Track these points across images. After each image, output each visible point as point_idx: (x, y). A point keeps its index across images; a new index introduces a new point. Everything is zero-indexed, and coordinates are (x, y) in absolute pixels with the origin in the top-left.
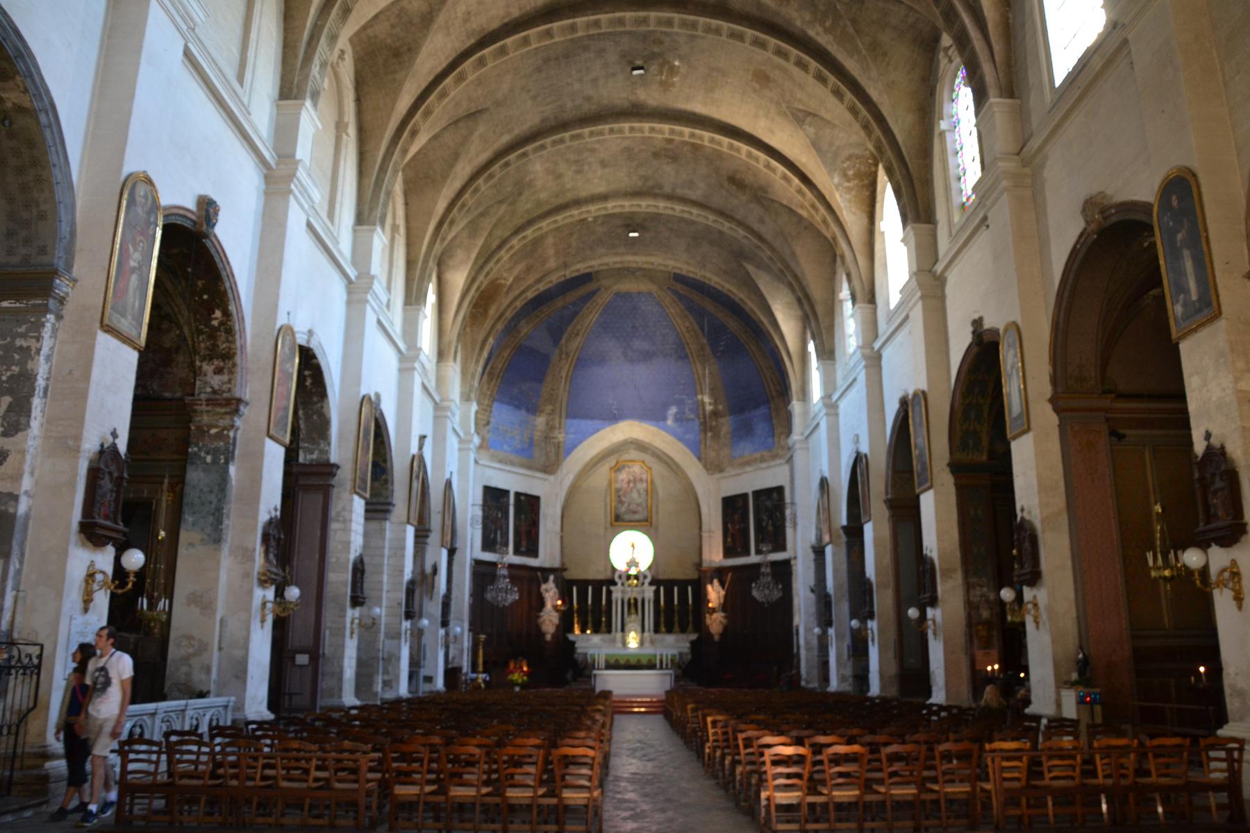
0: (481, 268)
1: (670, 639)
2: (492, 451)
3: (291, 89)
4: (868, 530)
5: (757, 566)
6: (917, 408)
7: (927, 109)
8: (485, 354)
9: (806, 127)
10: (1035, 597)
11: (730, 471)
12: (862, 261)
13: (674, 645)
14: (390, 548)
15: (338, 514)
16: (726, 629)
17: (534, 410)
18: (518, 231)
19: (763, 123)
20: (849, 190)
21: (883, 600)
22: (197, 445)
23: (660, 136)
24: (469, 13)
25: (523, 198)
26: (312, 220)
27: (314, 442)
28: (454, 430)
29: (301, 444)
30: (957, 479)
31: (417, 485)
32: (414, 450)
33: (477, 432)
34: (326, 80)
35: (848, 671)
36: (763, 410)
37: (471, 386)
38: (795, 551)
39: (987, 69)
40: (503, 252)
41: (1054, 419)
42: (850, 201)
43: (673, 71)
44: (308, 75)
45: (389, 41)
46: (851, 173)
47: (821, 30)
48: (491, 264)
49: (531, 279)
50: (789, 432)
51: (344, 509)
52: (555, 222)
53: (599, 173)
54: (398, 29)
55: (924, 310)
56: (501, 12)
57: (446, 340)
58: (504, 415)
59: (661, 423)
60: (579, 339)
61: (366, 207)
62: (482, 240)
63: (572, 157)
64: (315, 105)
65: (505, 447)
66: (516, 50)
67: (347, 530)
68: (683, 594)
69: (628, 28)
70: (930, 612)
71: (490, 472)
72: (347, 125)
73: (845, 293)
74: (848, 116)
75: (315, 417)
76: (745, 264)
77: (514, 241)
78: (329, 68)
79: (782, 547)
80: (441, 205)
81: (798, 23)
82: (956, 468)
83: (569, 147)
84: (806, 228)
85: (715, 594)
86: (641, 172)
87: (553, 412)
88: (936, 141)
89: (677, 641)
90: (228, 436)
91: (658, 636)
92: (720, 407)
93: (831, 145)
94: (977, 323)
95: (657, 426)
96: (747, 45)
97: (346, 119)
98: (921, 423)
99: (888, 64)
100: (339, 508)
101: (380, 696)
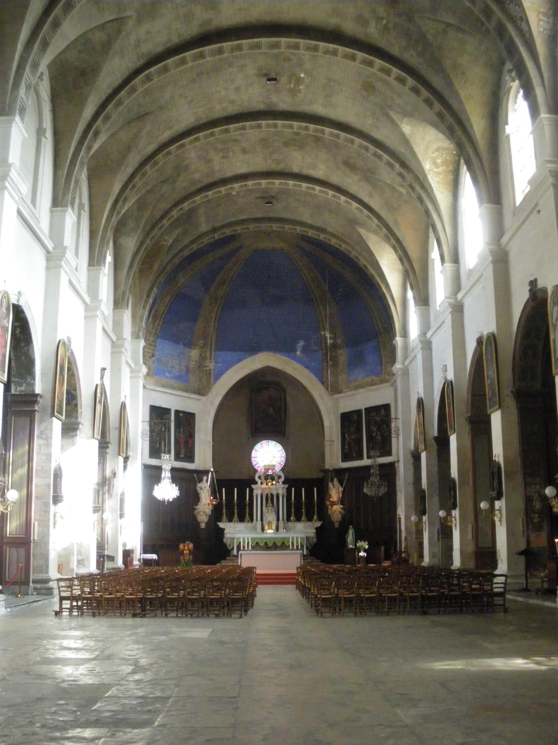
0: (147, 234)
1: (300, 526)
2: (156, 377)
4: (453, 439)
5: (367, 468)
8: (151, 301)
13: (302, 531)
16: (343, 517)
17: (189, 344)
18: (176, 205)
19: (370, 121)
20: (438, 174)
23: (290, 130)
25: (181, 178)
26: (21, 208)
28: (127, 362)
31: (99, 408)
32: (98, 381)
33: (145, 363)
34: (30, 99)
35: (438, 550)
37: (140, 327)
38: (398, 457)
39: (539, 91)
40: (165, 221)
42: (439, 183)
43: (299, 81)
44: (16, 97)
46: (439, 161)
47: (414, 54)
49: (186, 241)
50: (393, 360)
58: (166, 349)
59: (292, 354)
60: (225, 287)
61: (61, 193)
64: (22, 119)
65: (167, 374)
66: (176, 68)
68: (310, 495)
69: (264, 50)
71: (155, 395)
72: (45, 131)
73: (435, 255)
75: (23, 358)
78: (32, 90)
79: (389, 453)
80: (117, 188)
83: (217, 139)
85: (335, 492)
86: (274, 157)
87: (205, 346)
89: (305, 527)
91: (290, 524)
94: (533, 283)
95: (289, 357)
97: (44, 126)
98: (492, 360)
99: (466, 82)
101: (75, 572)
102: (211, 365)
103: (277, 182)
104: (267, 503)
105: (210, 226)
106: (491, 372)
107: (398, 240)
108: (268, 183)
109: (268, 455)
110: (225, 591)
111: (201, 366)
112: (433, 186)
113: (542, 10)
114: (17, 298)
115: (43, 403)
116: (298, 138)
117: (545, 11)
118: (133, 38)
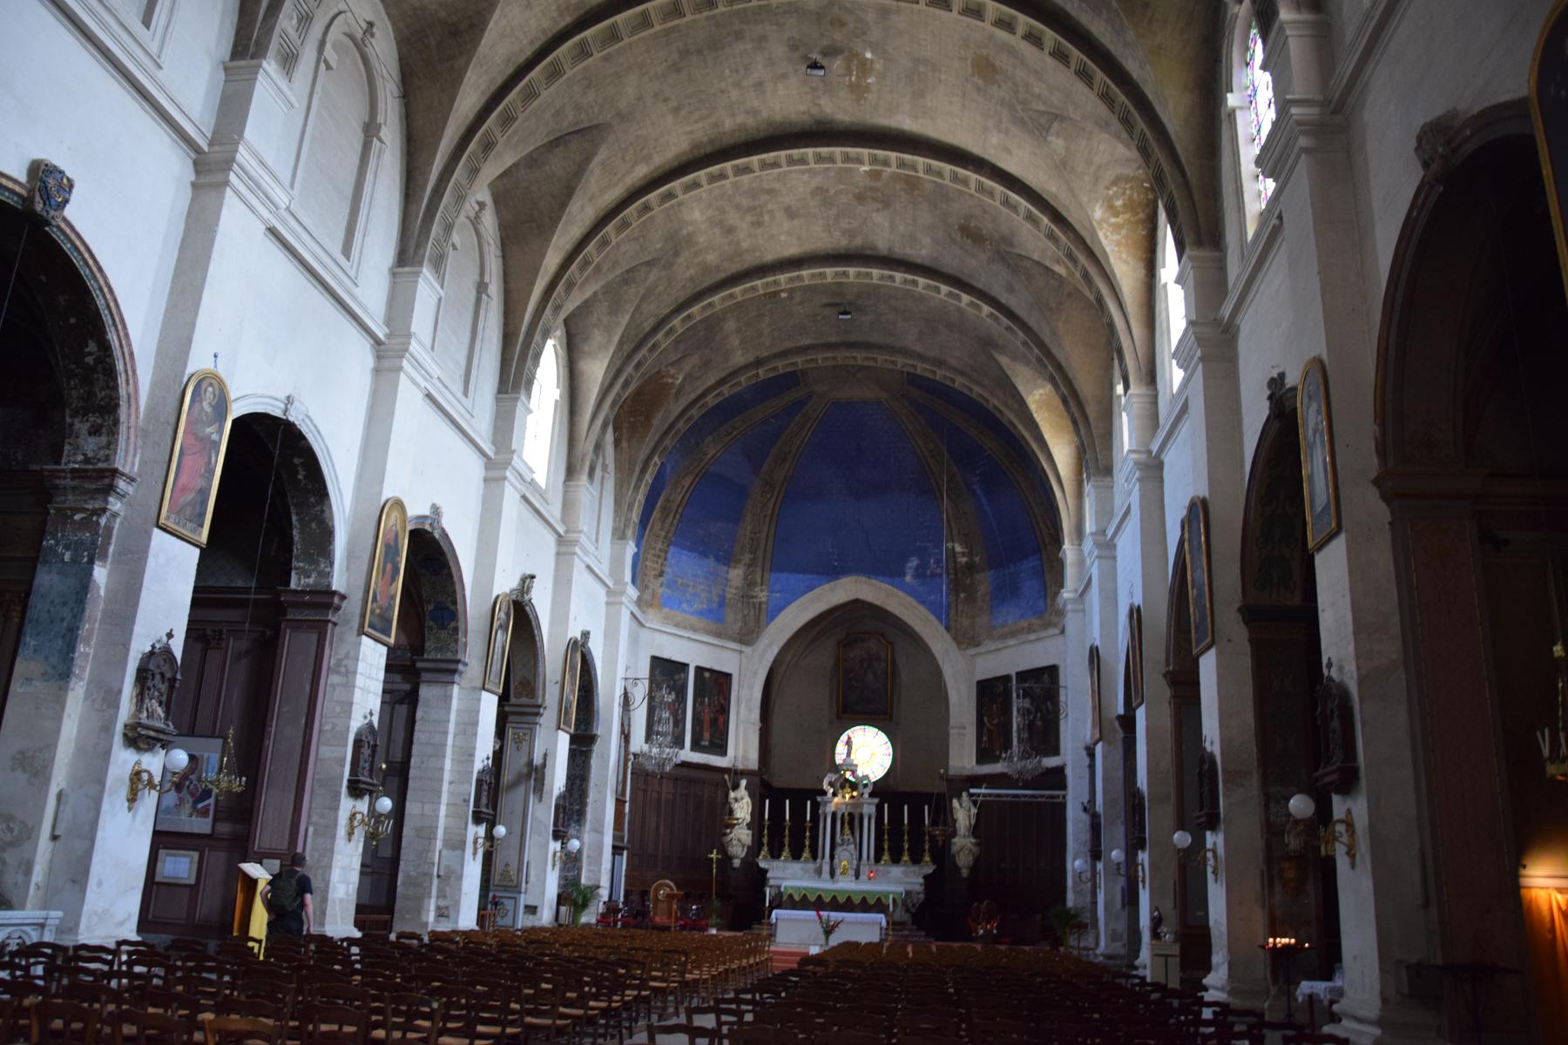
0: (629, 357)
1: (897, 871)
2: (666, 610)
3: (247, 46)
6: (1195, 525)
7: (1210, 84)
8: (649, 478)
9: (1052, 139)
10: (1349, 812)
11: (989, 645)
13: (899, 881)
15: (338, 664)
16: (976, 861)
17: (727, 559)
20: (1118, 227)
21: (1156, 819)
22: (54, 537)
25: (681, 260)
27: (312, 561)
29: (295, 563)
30: (1251, 630)
41: (1383, 513)
42: (1118, 244)
43: (865, 68)
45: (443, 14)
46: (1119, 203)
48: (644, 351)
49: (712, 379)
51: (347, 656)
55: (1205, 379)
57: (579, 451)
58: (684, 564)
59: (897, 580)
61: (413, 243)
62: (627, 317)
63: (745, 202)
65: (685, 606)
66: (632, 34)
67: (349, 686)
70: (1210, 838)
74: (1102, 109)
75: (314, 526)
77: (676, 321)
79: (1055, 751)
82: (1251, 614)
84: (1070, 295)
85: (963, 813)
86: (844, 224)
89: (905, 874)
90: (98, 524)
92: (977, 559)
93: (1089, 162)
98: (1199, 548)
100: (341, 655)
102: (762, 595)
103: (852, 270)
105: (751, 357)
106: (1198, 573)
107: (1059, 367)
108: (836, 274)
109: (868, 752)
110: (59, 981)
111: (746, 596)
115: (352, 608)
116: (878, 184)
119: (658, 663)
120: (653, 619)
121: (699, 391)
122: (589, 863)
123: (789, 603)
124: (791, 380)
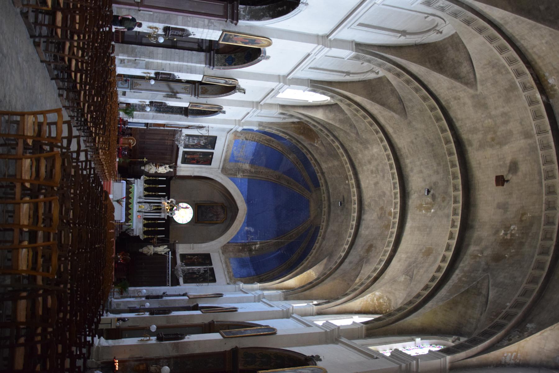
0: (324, 127)
1: (141, 226)
7: (424, 332)
8: (281, 134)
12: (336, 308)
13: (137, 227)
14: (191, 66)
15: (212, 23)
16: (145, 255)
17: (252, 163)
19: (404, 256)
20: (373, 301)
21: (161, 319)
24: (459, 99)
25: (359, 145)
29: (248, 7)
36: (253, 272)
37: (266, 127)
39: (462, 355)
40: (332, 138)
42: (367, 301)
45: (445, 58)
46: (381, 301)
47: (460, 276)
48: (326, 132)
49: (316, 156)
51: (215, 26)
52: (346, 163)
53: (372, 182)
54: (451, 62)
56: (459, 117)
58: (250, 148)
59: (246, 224)
61: (364, 48)
62: (338, 126)
63: (380, 168)
65: (235, 148)
67: (204, 27)
71: (223, 139)
74: (414, 294)
75: (262, 13)
76: (326, 258)
81: (461, 265)
82: (235, 351)
84: (348, 284)
85: (162, 249)
86: (372, 203)
88: (409, 338)
91: (142, 220)
93: (396, 290)
96: (447, 241)
99: (446, 310)
102: (239, 176)
103: (356, 206)
104: (156, 206)
105: (324, 170)
106: (249, 332)
107: (323, 281)
108: (355, 201)
109: (184, 215)
111: (239, 170)
112: (365, 297)
113: (519, 354)
114: (304, 2)
115: (232, 27)
116: (387, 215)
117: (518, 356)
118: (462, 94)
119: (215, 138)
120: (230, 136)
121: (312, 152)
122: (141, 115)
123: (237, 185)
124: (317, 184)
